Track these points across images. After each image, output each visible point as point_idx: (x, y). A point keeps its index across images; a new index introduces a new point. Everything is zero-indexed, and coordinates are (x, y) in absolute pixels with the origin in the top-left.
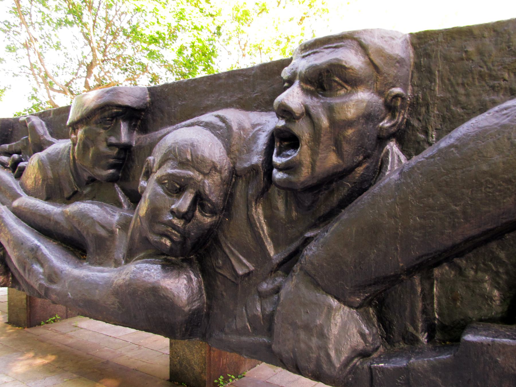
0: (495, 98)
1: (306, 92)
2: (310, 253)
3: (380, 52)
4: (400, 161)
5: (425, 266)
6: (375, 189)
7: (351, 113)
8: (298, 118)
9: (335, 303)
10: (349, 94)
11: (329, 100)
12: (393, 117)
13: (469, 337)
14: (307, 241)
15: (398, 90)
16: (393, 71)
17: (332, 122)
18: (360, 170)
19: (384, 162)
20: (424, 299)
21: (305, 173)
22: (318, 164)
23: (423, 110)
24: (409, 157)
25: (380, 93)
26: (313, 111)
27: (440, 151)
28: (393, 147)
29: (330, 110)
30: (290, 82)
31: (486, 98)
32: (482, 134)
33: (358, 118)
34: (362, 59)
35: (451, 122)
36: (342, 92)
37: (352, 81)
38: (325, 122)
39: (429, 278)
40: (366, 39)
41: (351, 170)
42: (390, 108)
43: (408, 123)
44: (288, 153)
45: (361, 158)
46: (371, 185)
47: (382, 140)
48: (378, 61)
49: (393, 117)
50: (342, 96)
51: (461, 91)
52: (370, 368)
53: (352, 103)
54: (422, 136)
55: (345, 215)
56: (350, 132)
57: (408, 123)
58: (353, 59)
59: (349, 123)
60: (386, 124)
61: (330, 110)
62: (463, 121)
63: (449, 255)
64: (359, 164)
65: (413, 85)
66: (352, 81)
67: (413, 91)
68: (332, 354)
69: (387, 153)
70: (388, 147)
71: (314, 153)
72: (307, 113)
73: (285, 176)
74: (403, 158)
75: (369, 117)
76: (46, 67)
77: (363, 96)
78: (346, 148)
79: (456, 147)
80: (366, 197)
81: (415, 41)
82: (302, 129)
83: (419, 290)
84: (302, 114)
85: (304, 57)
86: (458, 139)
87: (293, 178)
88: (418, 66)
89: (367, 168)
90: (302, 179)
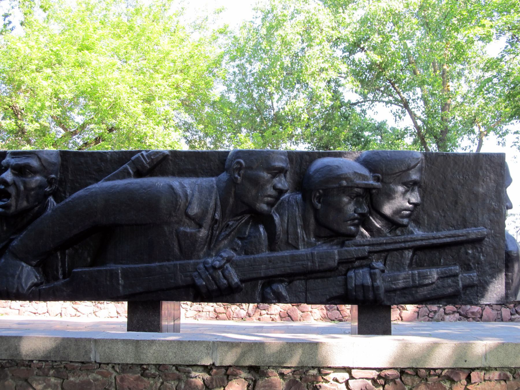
0: (90, 181)
1: (14, 174)
2: (14, 244)
3: (46, 160)
4: (54, 205)
5: (63, 247)
6: (43, 216)
7: (33, 185)
8: (10, 186)
9: (24, 264)
10: (32, 177)
11: (24, 179)
12: (51, 187)
13: (75, 270)
14: (12, 240)
15: (53, 176)
16: (51, 168)
17: (25, 187)
18: (36, 209)
19: (47, 205)
20: (62, 261)
21: (13, 209)
22: (19, 205)
23: (64, 183)
24: (57, 202)
25: (46, 177)
26: (17, 183)
27: (66, 203)
28: (51, 199)
29: (25, 183)
30: (6, 169)
31: (88, 181)
32: (80, 197)
33: (36, 187)
34: (39, 163)
35: (75, 189)
36: (30, 176)
37: (34, 172)
38: (22, 188)
39: (63, 255)
40: (41, 155)
41: (32, 208)
42: (50, 182)
43: (58, 188)
44: (5, 200)
45: (37, 203)
46: (41, 215)
47: (46, 196)
48: (44, 164)
49: (51, 187)
50: (30, 178)
51: (78, 177)
52: (39, 290)
53: (34, 181)
54: (63, 195)
55: (30, 228)
56: (33, 193)
57: (58, 188)
58: (34, 163)
59: (33, 189)
60: (48, 189)
61: (25, 183)
62: (79, 190)
63: (63, 247)
64: (36, 206)
65: (60, 173)
66: (34, 172)
67: (60, 175)
68: (24, 285)
69: (49, 201)
70: (49, 199)
71: (17, 201)
72: (14, 183)
73: (3, 210)
74: (55, 203)
75: (41, 186)
76: (494, 365)
77: (38, 178)
78: (31, 199)
79: (71, 201)
80: (39, 220)
81: (62, 154)
82: (12, 190)
83: (60, 257)
84: (12, 184)
85: (13, 158)
86: (72, 199)
87: (8, 212)
88: (62, 165)
89: (39, 208)
90: (11, 212)
